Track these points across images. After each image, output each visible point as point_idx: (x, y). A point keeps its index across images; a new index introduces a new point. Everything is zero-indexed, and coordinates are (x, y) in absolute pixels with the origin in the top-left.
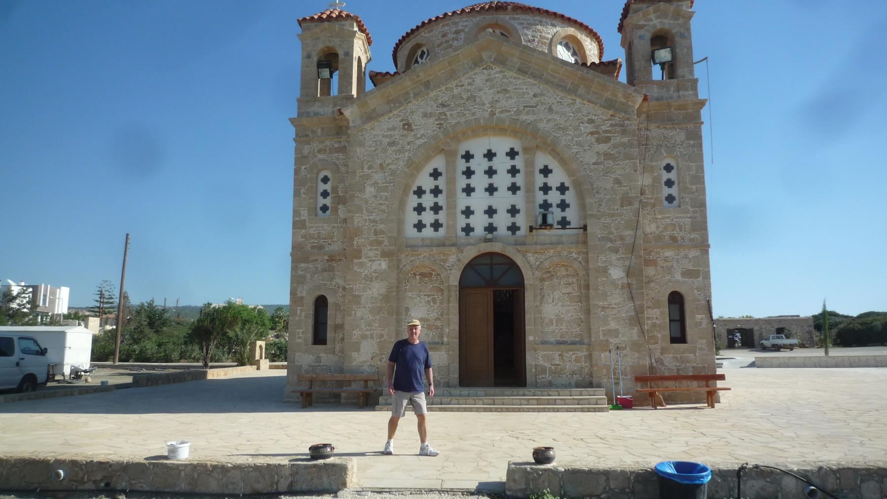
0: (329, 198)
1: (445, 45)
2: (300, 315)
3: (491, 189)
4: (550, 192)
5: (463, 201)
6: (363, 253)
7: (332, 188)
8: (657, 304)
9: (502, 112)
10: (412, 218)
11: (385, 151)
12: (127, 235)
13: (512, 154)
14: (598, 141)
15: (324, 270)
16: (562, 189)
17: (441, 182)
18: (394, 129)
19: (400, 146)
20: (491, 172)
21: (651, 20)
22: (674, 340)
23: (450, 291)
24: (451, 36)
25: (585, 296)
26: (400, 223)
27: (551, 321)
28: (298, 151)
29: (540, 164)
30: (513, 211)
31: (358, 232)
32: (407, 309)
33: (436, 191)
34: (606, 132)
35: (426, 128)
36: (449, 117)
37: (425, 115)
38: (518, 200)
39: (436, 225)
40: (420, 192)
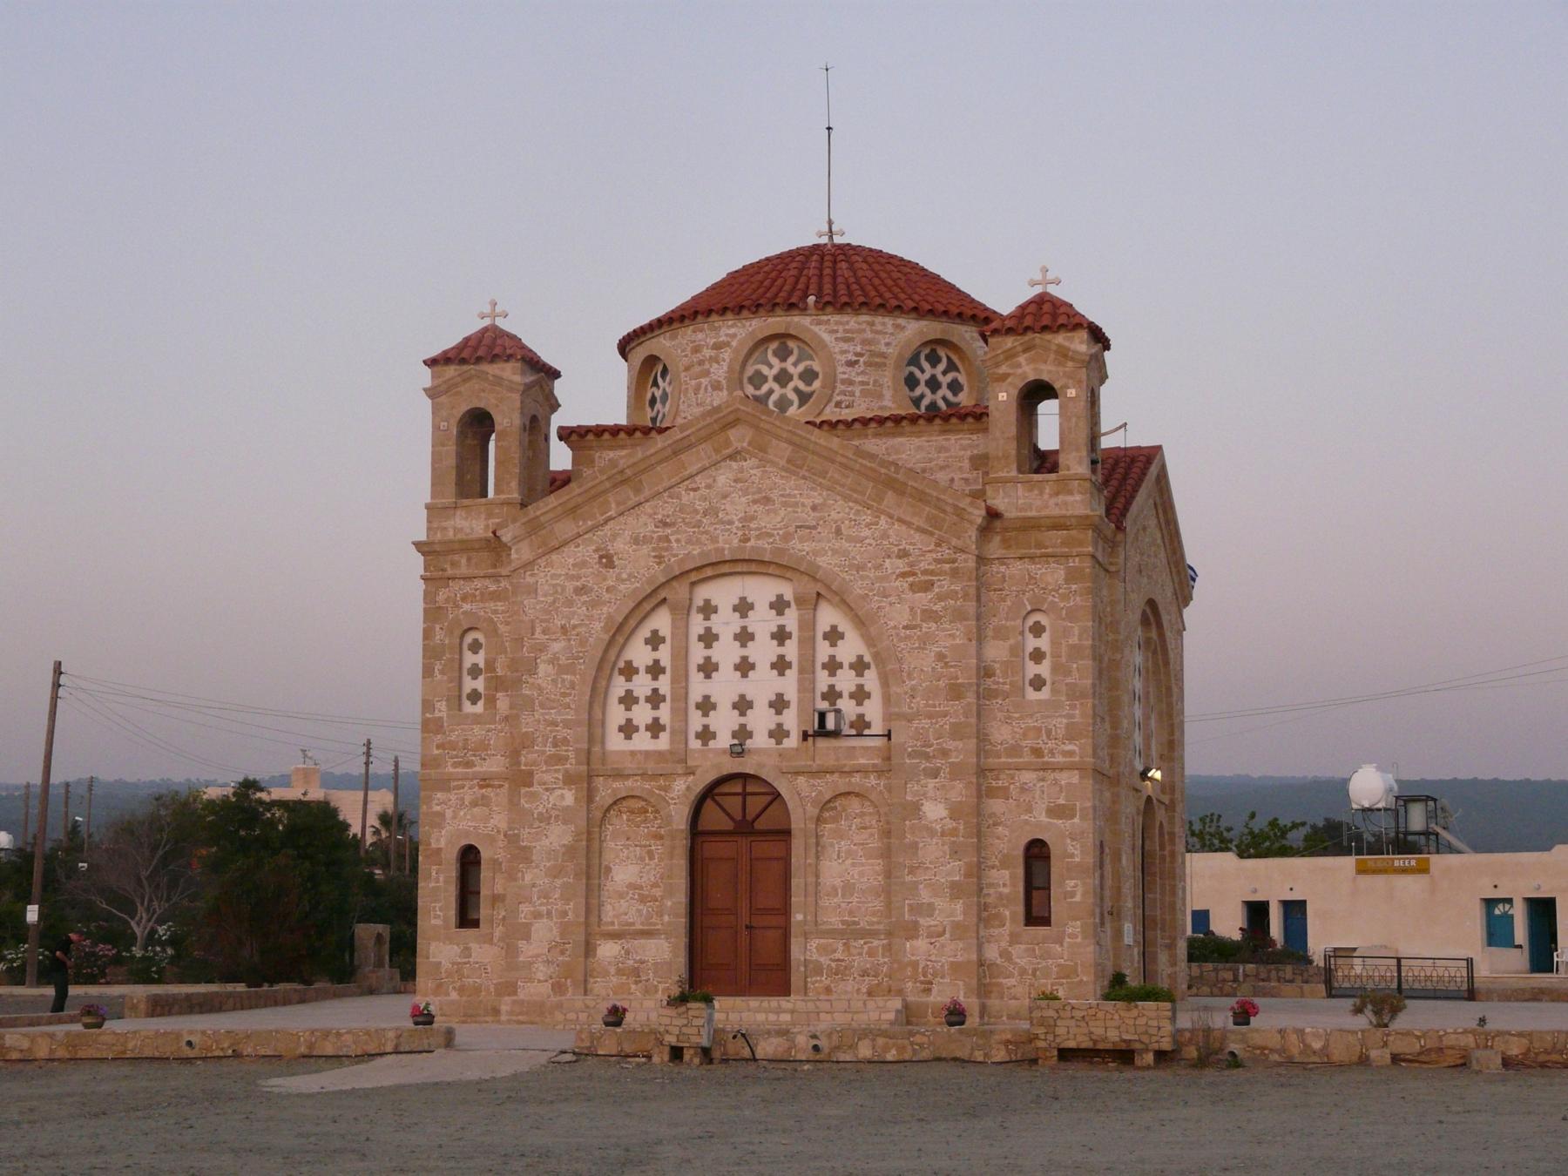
0: (481, 678)
1: (697, 369)
3: (745, 667)
4: (839, 672)
7: (487, 662)
8: (1005, 864)
9: (758, 537)
11: (570, 603)
12: (58, 670)
13: (779, 606)
14: (913, 588)
15: (474, 804)
16: (860, 666)
18: (583, 564)
21: (1019, 366)
25: (893, 847)
27: (835, 889)
28: (429, 597)
29: (823, 625)
30: (779, 704)
32: (609, 870)
34: (925, 572)
35: (638, 568)
36: (675, 545)
37: (636, 541)
38: (789, 685)
39: (655, 728)
40: (629, 671)
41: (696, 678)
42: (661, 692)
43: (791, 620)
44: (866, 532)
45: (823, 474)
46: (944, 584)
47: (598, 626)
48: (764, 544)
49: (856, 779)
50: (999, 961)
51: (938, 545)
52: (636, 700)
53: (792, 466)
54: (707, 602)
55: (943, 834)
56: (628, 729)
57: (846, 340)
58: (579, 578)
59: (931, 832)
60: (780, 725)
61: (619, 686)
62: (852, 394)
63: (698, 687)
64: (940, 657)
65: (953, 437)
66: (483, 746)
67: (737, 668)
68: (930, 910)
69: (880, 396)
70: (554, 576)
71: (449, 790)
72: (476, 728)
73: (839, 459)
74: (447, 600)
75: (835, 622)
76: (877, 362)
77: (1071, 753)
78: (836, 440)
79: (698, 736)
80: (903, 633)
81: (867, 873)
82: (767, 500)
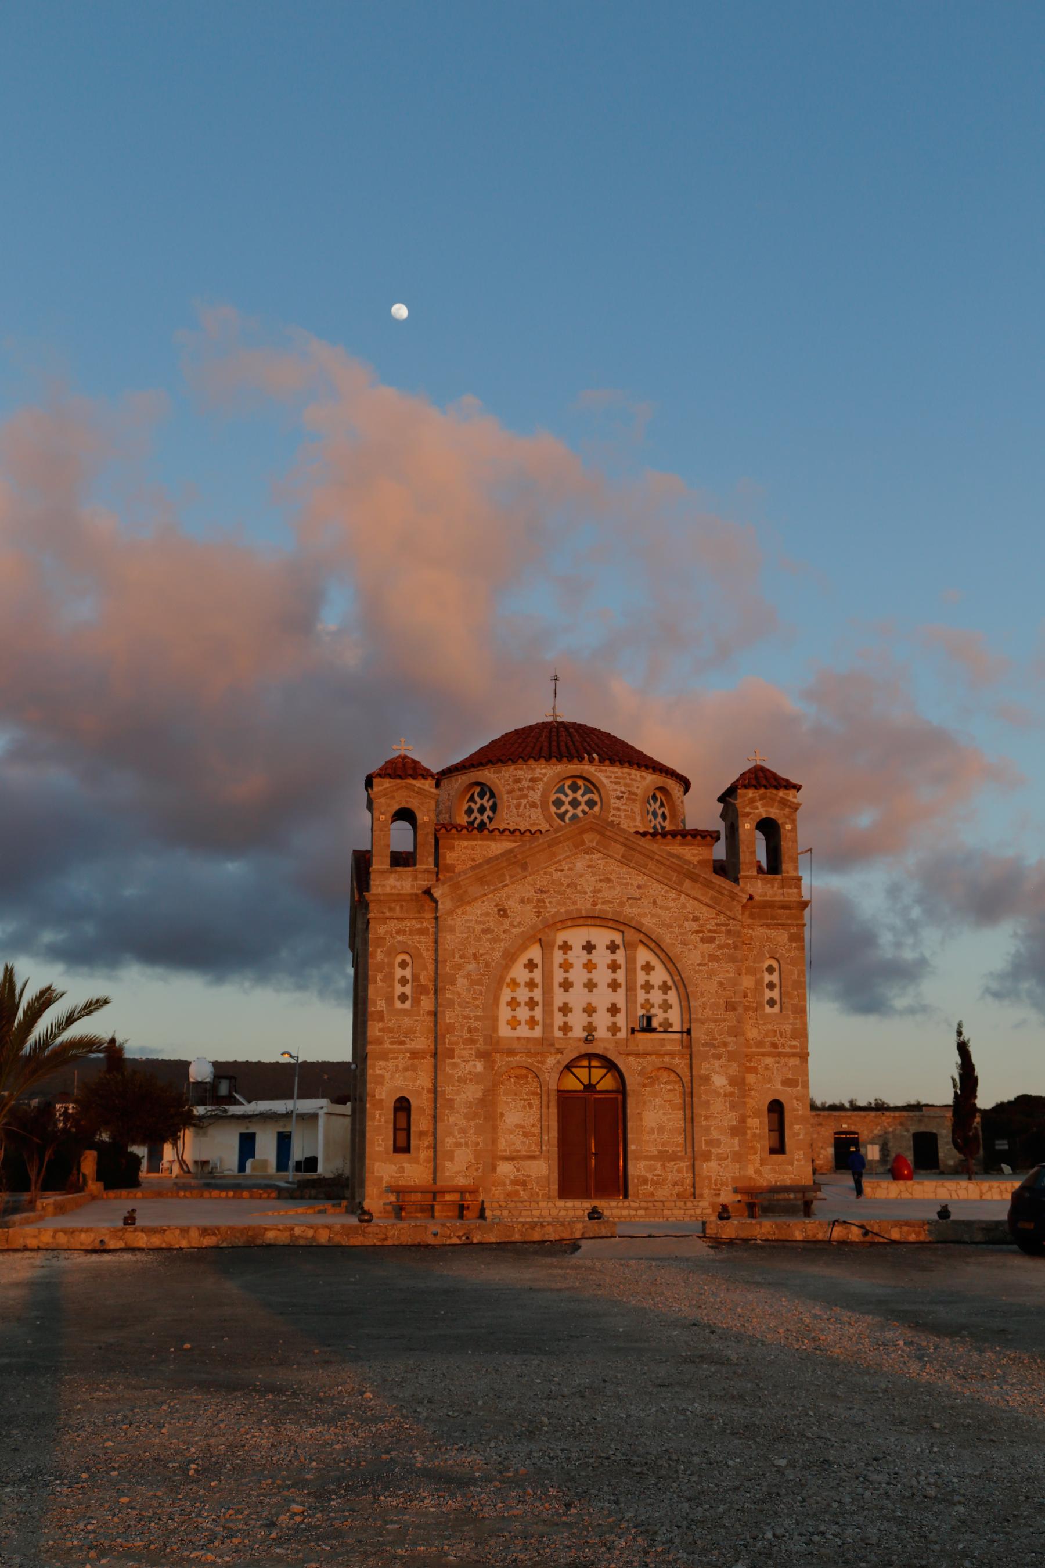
1: (518, 793)
2: (380, 1121)
6: (456, 1053)
8: (756, 1114)
13: (613, 947)
14: (702, 940)
15: (406, 1069)
16: (665, 988)
18: (488, 914)
19: (494, 935)
21: (757, 808)
22: (773, 1151)
23: (549, 1095)
24: (526, 784)
26: (495, 1019)
29: (641, 961)
30: (614, 1010)
31: (450, 1029)
32: (502, 1114)
34: (710, 931)
35: (524, 916)
39: (532, 1022)
40: (514, 983)
41: (558, 991)
42: (536, 999)
43: (620, 956)
44: (672, 904)
45: (645, 866)
46: (722, 939)
47: (498, 955)
48: (606, 907)
49: (667, 1059)
50: (754, 1176)
51: (717, 914)
52: (519, 1004)
53: (625, 861)
54: (565, 942)
55: (725, 1095)
56: (514, 1023)
57: (618, 783)
58: (484, 923)
59: (718, 1094)
60: (614, 1024)
61: (506, 995)
62: (620, 817)
63: (559, 997)
64: (721, 984)
65: (687, 848)
66: (410, 1032)
67: (585, 986)
68: (717, 1143)
69: (634, 819)
70: (467, 921)
71: (387, 1059)
72: (407, 1019)
73: (657, 857)
74: (386, 932)
75: (648, 959)
76: (632, 797)
77: (794, 1047)
78: (655, 845)
79: (560, 1029)
80: (697, 968)
81: (675, 1119)
82: (608, 880)
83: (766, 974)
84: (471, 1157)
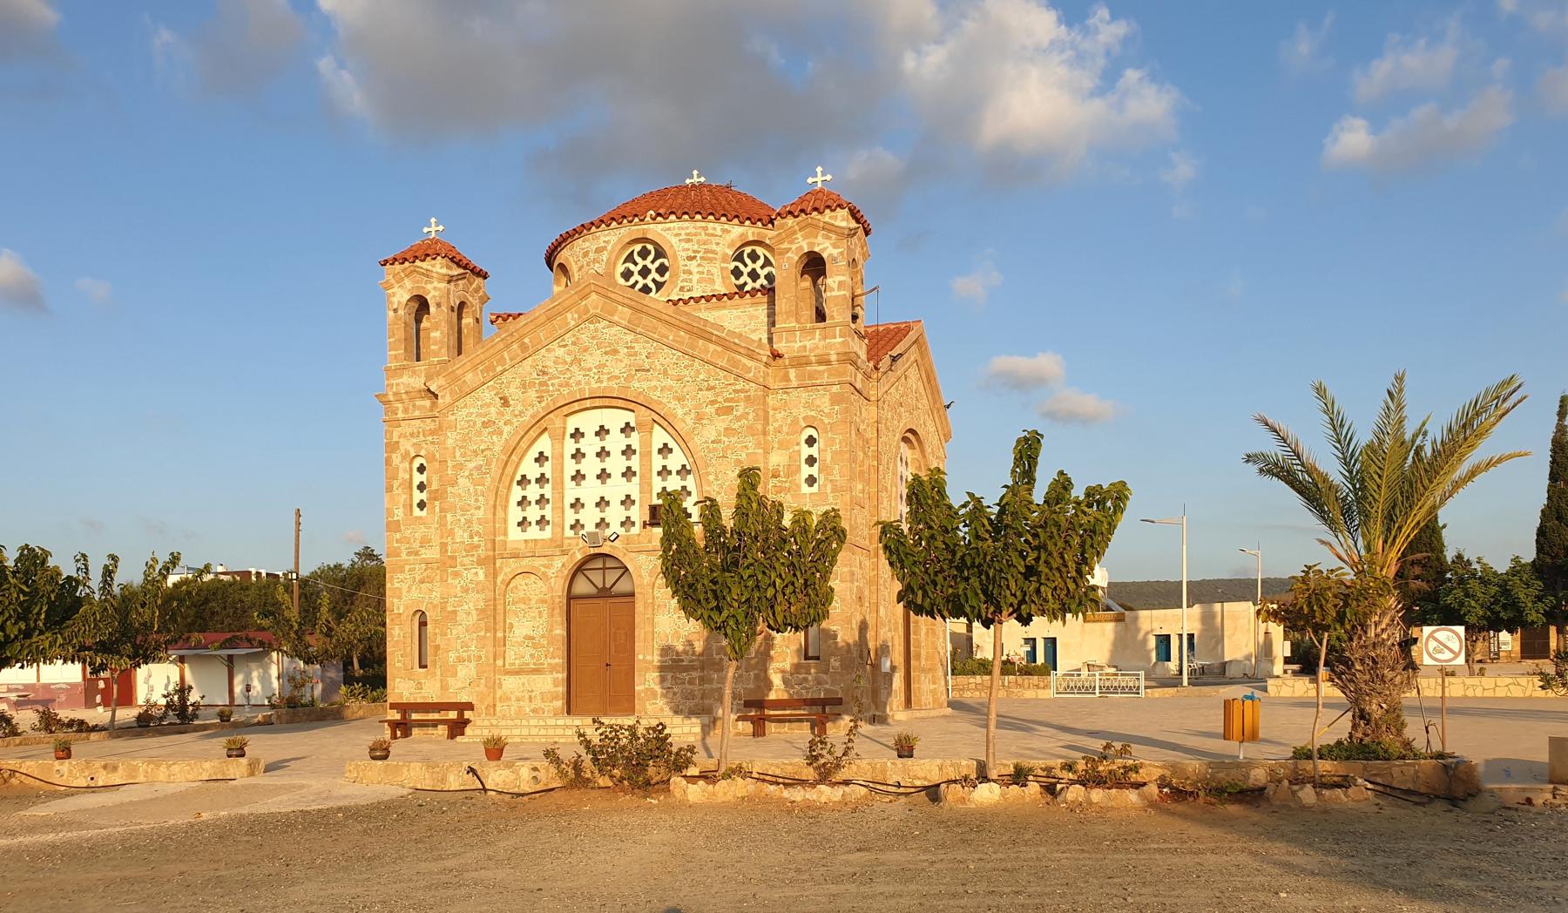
3: (603, 475)
5: (571, 492)
10: (515, 514)
11: (479, 434)
17: (547, 469)
20: (603, 454)
24: (592, 256)
33: (541, 480)
35: (527, 405)
38: (633, 488)
39: (542, 522)
40: (524, 481)
43: (634, 440)
48: (613, 384)
57: (688, 241)
69: (713, 282)
82: (615, 352)
83: (804, 446)
84: (473, 672)
